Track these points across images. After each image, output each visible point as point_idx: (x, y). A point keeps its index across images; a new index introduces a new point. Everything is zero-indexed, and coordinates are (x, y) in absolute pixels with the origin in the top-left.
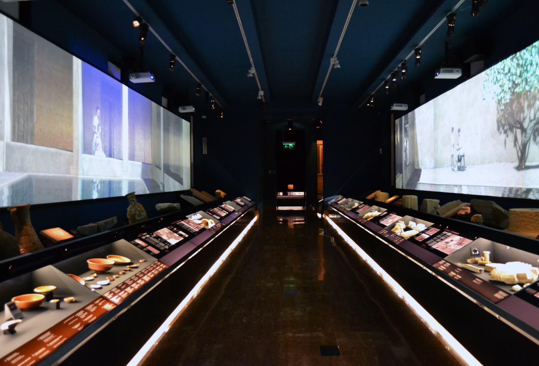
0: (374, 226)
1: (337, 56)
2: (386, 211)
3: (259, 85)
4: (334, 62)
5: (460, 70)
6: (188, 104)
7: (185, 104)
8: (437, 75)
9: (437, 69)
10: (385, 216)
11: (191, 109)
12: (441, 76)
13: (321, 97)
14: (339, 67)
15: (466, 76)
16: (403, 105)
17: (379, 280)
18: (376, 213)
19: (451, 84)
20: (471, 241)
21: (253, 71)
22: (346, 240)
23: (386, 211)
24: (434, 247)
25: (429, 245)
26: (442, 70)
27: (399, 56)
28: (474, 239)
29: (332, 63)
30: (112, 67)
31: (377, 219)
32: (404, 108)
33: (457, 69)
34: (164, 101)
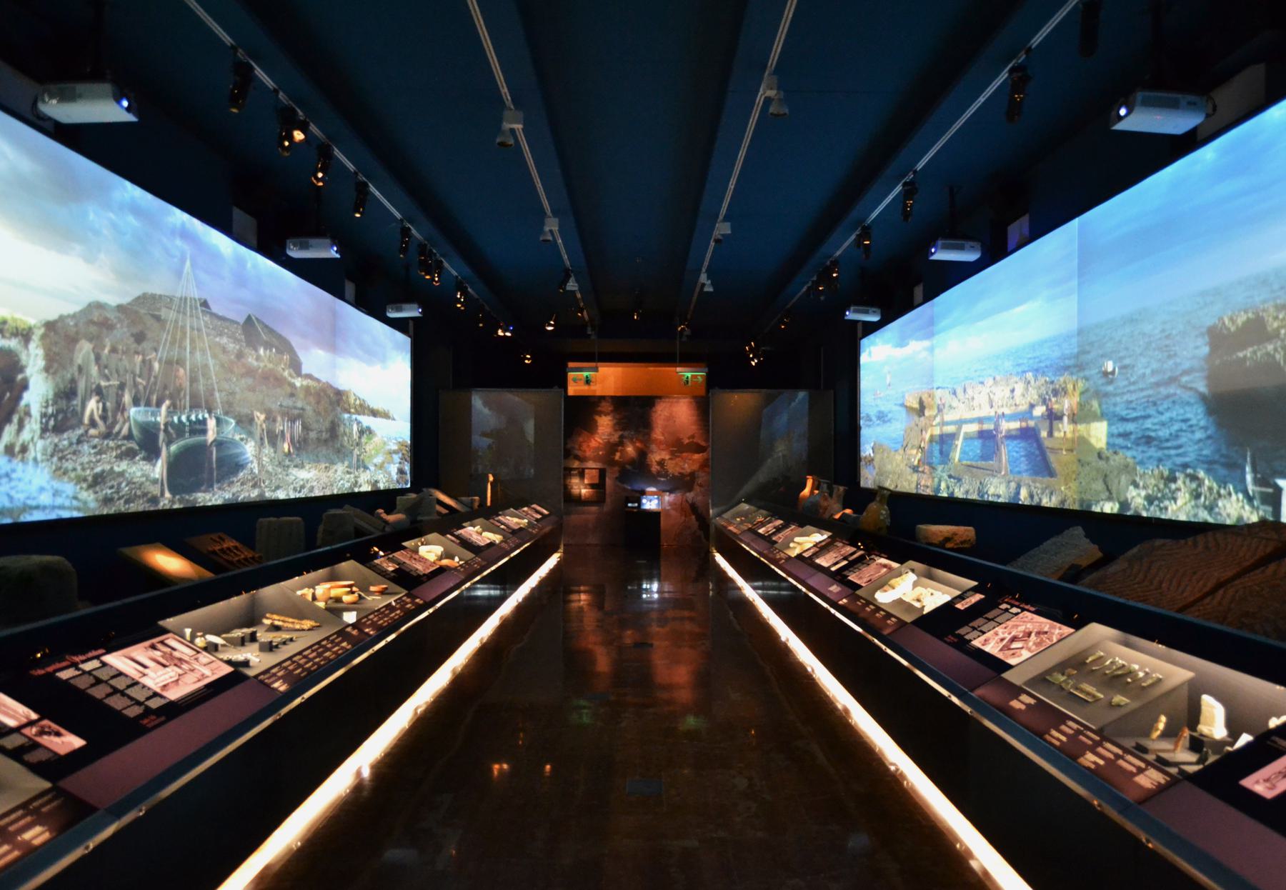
0: (803, 571)
1: (707, 271)
2: (975, 590)
3: (505, 90)
4: (723, 229)
5: (879, 311)
6: (318, 233)
7: (400, 301)
8: (1120, 118)
9: (931, 241)
10: (976, 612)
11: (411, 312)
12: (941, 255)
13: (726, 219)
14: (711, 290)
15: (995, 251)
16: (872, 310)
17: (894, 781)
18: (932, 597)
19: (962, 272)
20: (1067, 630)
21: (552, 225)
22: (783, 639)
23: (975, 590)
24: (977, 643)
25: (967, 637)
26: (940, 242)
27: (854, 214)
28: (1078, 625)
29: (760, 100)
30: (238, 215)
31: (944, 622)
32: (969, 256)
33: (972, 243)
34: (350, 288)
